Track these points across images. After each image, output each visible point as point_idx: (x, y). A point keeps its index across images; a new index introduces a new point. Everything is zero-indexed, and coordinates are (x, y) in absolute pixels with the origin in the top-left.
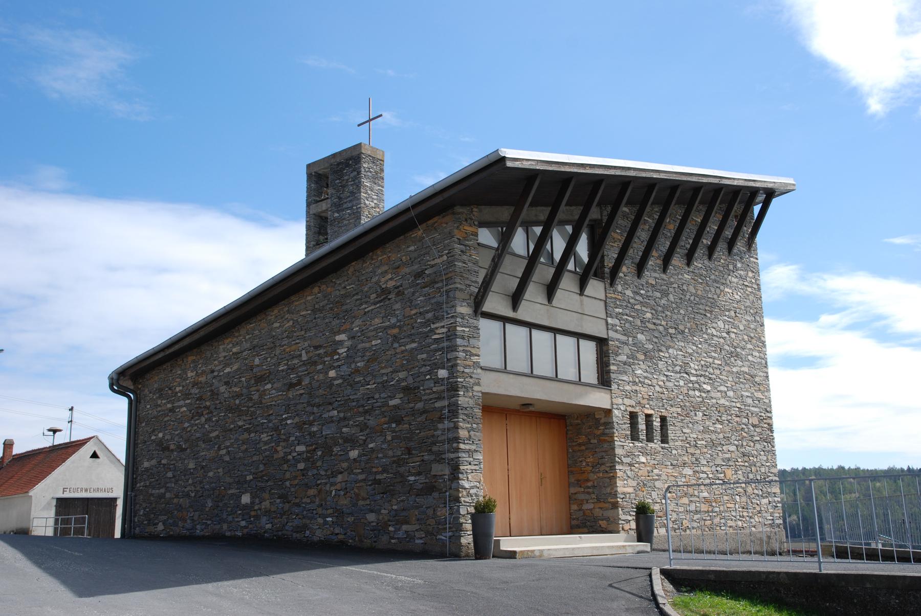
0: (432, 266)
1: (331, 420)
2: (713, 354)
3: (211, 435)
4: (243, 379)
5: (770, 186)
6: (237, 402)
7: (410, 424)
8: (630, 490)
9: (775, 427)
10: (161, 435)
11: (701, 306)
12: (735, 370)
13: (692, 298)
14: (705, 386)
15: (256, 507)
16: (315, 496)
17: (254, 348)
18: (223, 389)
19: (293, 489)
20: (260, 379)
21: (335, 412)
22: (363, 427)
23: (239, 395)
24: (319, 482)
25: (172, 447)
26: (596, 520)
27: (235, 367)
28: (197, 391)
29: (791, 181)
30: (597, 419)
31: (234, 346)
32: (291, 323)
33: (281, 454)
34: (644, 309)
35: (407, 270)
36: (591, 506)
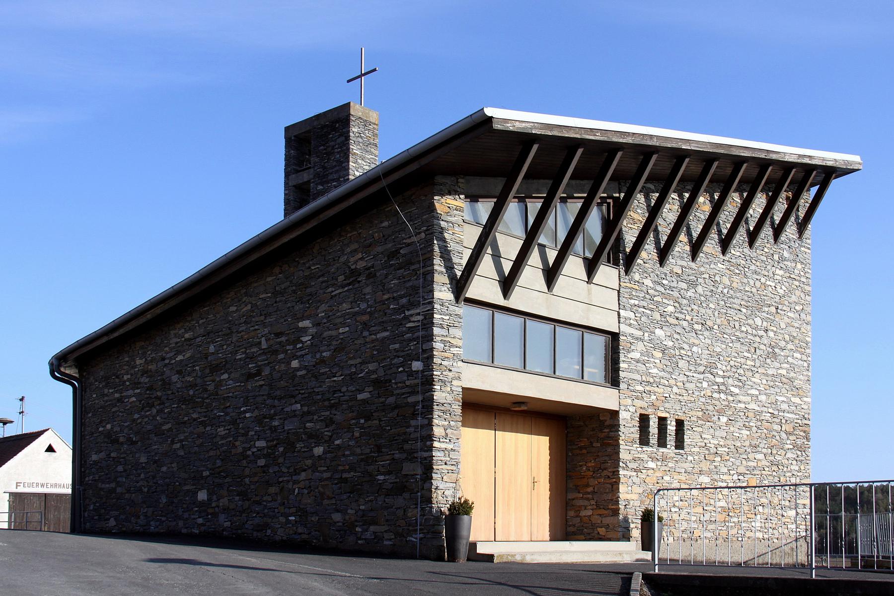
0: (409, 245)
1: (294, 414)
2: (746, 354)
3: (164, 428)
4: (197, 368)
5: (830, 164)
6: (191, 392)
7: (380, 420)
8: (635, 497)
9: (811, 436)
10: (109, 426)
11: (735, 301)
12: (770, 372)
13: (725, 291)
14: (733, 389)
15: (214, 505)
16: (276, 494)
17: (208, 334)
18: (175, 378)
19: (252, 487)
20: (215, 369)
21: (298, 406)
22: (329, 422)
23: (193, 386)
24: (281, 479)
25: (121, 439)
26: (594, 526)
27: (188, 355)
28: (147, 380)
29: (856, 158)
30: (601, 421)
31: (186, 332)
32: (249, 307)
33: (240, 450)
34: (665, 301)
35: (380, 249)
36: (589, 513)
